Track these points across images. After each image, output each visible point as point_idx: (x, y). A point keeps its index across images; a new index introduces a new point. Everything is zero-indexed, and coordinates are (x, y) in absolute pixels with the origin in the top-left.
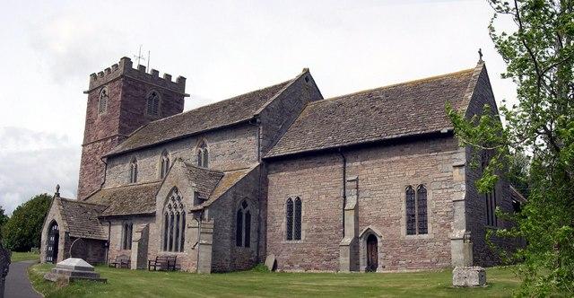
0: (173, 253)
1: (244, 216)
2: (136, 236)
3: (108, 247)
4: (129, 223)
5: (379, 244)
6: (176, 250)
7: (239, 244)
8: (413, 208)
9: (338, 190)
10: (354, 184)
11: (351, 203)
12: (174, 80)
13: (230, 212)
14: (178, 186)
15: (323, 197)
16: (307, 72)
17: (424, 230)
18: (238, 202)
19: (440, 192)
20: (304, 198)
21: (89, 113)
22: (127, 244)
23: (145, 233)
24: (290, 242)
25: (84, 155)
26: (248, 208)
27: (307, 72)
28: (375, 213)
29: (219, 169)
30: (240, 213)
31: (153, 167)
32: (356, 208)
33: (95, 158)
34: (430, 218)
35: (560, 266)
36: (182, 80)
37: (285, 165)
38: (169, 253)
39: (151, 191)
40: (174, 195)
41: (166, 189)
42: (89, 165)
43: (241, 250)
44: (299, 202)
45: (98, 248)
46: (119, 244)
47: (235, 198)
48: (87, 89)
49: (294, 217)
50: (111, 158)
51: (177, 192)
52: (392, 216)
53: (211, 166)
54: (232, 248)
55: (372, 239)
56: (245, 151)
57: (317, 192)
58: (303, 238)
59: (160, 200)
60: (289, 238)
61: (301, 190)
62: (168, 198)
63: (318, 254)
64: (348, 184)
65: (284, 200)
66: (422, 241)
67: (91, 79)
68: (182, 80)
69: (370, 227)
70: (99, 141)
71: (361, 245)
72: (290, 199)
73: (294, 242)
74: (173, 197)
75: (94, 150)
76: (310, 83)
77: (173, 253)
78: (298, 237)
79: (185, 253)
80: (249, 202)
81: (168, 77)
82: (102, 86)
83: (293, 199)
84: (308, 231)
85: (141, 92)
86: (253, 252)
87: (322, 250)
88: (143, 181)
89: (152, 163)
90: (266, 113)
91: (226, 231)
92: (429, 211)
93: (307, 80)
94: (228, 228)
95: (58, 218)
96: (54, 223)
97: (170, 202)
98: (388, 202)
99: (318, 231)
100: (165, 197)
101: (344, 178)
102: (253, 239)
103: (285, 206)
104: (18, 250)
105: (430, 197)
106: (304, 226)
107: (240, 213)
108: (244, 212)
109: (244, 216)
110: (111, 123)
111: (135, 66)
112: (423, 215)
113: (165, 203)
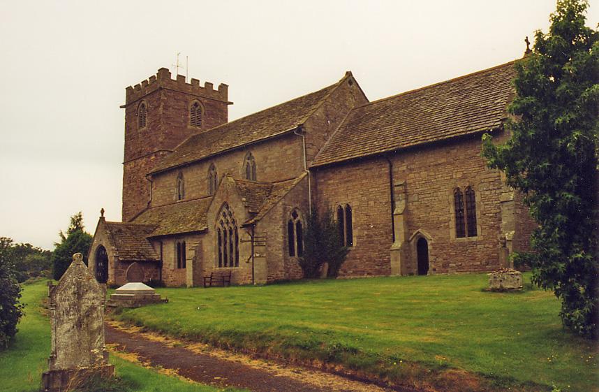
1: (295, 227)
2: (190, 254)
4: (181, 241)
5: (430, 247)
6: (225, 266)
7: (292, 254)
9: (386, 195)
10: (401, 188)
12: (216, 88)
13: (281, 223)
15: (372, 203)
16: (349, 74)
17: (473, 232)
19: (487, 193)
20: (354, 204)
23: (199, 251)
26: (299, 218)
27: (349, 74)
30: (291, 224)
32: (407, 212)
34: (479, 221)
36: (224, 87)
44: (348, 208)
46: (173, 264)
50: (157, 175)
52: (440, 219)
55: (422, 243)
58: (354, 244)
62: (219, 214)
63: (370, 259)
64: (396, 189)
66: (471, 243)
68: (224, 87)
73: (465, 239)
80: (299, 213)
81: (209, 85)
82: (141, 99)
83: (343, 206)
84: (359, 237)
85: (183, 103)
87: (374, 255)
92: (478, 213)
94: (280, 239)
97: (222, 218)
100: (216, 212)
101: (391, 182)
105: (477, 199)
106: (355, 233)
107: (291, 224)
108: (295, 222)
109: (295, 227)
111: (174, 77)
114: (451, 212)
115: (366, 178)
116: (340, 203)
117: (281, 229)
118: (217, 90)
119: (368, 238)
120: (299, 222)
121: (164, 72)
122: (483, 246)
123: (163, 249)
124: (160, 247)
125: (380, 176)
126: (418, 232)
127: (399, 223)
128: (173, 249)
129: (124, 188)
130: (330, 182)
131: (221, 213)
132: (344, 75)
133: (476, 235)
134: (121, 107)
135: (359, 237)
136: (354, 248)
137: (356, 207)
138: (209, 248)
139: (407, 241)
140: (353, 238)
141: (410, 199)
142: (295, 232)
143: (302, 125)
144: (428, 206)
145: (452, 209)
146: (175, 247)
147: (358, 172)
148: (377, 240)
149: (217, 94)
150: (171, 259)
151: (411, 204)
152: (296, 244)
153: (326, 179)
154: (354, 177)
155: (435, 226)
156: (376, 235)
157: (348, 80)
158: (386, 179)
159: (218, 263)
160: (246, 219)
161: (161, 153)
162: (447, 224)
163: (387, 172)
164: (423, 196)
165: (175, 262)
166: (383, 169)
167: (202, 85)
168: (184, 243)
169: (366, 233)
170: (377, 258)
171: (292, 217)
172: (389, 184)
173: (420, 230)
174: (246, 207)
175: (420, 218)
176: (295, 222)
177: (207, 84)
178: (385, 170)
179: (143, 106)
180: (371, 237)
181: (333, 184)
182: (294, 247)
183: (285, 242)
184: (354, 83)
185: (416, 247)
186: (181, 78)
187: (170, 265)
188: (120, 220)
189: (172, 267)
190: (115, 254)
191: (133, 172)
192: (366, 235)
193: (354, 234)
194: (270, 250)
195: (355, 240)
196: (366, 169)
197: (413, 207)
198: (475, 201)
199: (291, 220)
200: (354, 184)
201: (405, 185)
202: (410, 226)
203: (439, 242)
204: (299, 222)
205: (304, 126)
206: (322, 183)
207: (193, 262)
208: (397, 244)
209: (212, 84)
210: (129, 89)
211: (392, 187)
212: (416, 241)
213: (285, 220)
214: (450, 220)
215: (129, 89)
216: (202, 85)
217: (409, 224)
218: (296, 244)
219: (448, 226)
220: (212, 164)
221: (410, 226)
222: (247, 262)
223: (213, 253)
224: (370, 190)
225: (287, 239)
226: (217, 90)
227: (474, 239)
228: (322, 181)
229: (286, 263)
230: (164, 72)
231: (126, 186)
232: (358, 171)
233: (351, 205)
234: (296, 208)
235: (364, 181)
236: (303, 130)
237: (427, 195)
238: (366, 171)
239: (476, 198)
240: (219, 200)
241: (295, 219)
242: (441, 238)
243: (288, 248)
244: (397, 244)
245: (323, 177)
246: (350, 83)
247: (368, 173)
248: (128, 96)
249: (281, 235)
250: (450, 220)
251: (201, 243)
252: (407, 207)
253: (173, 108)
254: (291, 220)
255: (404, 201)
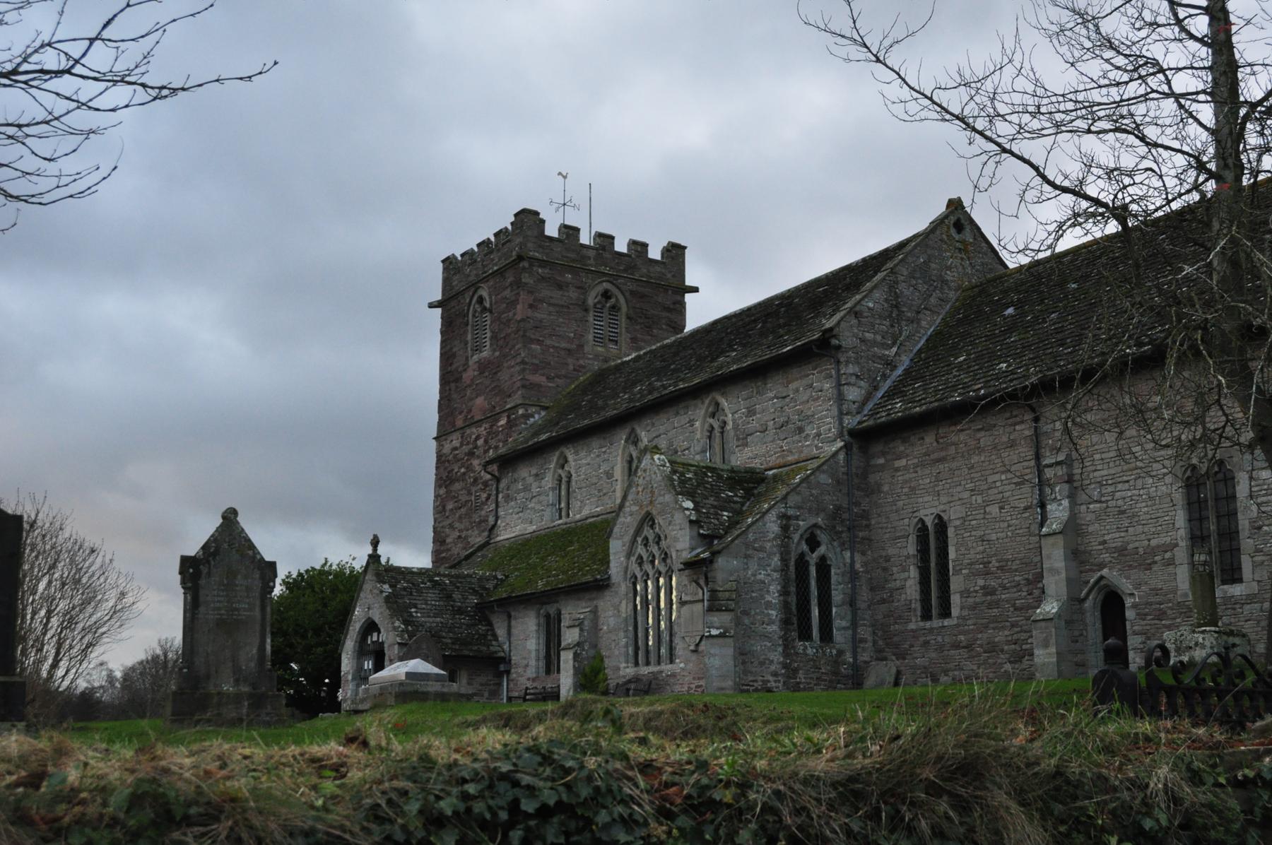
0: (653, 669)
1: (813, 571)
2: (570, 636)
3: (508, 672)
4: (552, 610)
5: (1130, 614)
6: (648, 663)
7: (805, 635)
8: (1202, 519)
9: (1026, 489)
10: (1060, 471)
11: (1058, 512)
12: (655, 253)
13: (776, 561)
14: (654, 512)
15: (994, 510)
16: (955, 205)
18: (796, 537)
20: (954, 515)
21: (447, 358)
22: (551, 664)
23: (592, 629)
24: (928, 624)
25: (441, 460)
26: (822, 550)
27: (955, 205)
28: (1114, 538)
29: (756, 464)
30: (802, 563)
31: (609, 475)
32: (1073, 528)
33: (470, 468)
34: (1247, 543)
35: (985, 652)
36: (675, 252)
37: (904, 441)
38: (645, 670)
39: (598, 531)
40: (647, 532)
41: (627, 521)
42: (457, 486)
43: (807, 649)
44: (941, 526)
45: (482, 679)
46: (533, 663)
47: (785, 528)
48: (437, 296)
49: (933, 565)
50: (509, 462)
51: (652, 527)
52: (1154, 543)
53: (741, 458)
54: (787, 646)
55: (1112, 604)
56: (809, 419)
57: (979, 499)
58: (955, 612)
59: (617, 547)
60: (926, 616)
61: (944, 499)
62: (634, 541)
63: (992, 648)
64: (1049, 473)
65: (907, 525)
67: (445, 269)
68: (675, 252)
69: (1105, 572)
70: (478, 423)
71: (1089, 619)
72: (922, 521)
73: (936, 623)
74: (646, 539)
75: (466, 449)
76: (968, 235)
77: (653, 669)
78: (946, 613)
79: (679, 665)
80: (822, 537)
81: (639, 247)
82: (475, 286)
83: (929, 522)
84: (965, 593)
85: (573, 294)
86: (840, 653)
87: (1000, 637)
88: (586, 512)
89: (604, 467)
90: (854, 321)
91: (769, 605)
92: (1243, 523)
93: (959, 227)
94: (773, 596)
95: (378, 614)
96: (371, 627)
97: (640, 550)
98: (1142, 508)
99: (987, 591)
100: (627, 538)
101: (1038, 457)
102: (840, 622)
103: (912, 539)
104: (1127, 667)
106: (956, 583)
107: (802, 563)
108: (813, 558)
109: (813, 571)
110: (504, 376)
111: (552, 230)
112: (1229, 535)
113: (629, 555)
114: (1177, 526)
115: (980, 450)
116: (921, 514)
117: (776, 575)
118: (658, 257)
119: (985, 594)
120: (823, 559)
121: (528, 220)
122: (1257, 606)
123: (514, 631)
124: (506, 624)
125: (1012, 445)
126: (1102, 578)
127: (1055, 558)
128: (534, 628)
129: (437, 496)
130: (898, 464)
131: (639, 540)
132: (944, 209)
133: (1240, 580)
134: (431, 306)
135: (965, 593)
136: (955, 622)
137: (958, 523)
138: (612, 621)
139: (1074, 601)
140: (952, 597)
141: (1082, 497)
142: (813, 583)
143: (831, 329)
144: (1123, 512)
145: (1181, 518)
146: (539, 625)
147: (962, 437)
148: (1007, 601)
149: (658, 269)
150: (530, 652)
151: (1083, 508)
152: (815, 612)
153: (889, 457)
154: (952, 450)
155: (1145, 560)
156: (1005, 588)
157: (953, 219)
158: (1026, 451)
159: (632, 659)
160: (693, 549)
161: (521, 412)
162: (1168, 555)
163: (1027, 433)
164: (1110, 489)
165: (538, 660)
166: (1017, 427)
167: (621, 246)
168: (559, 614)
169: (981, 582)
170: (1008, 643)
171: (805, 547)
172: (1033, 463)
173: (1105, 572)
174: (691, 522)
175: (1105, 542)
176: (813, 558)
177: (633, 244)
178: (1025, 430)
179: (481, 300)
180: (992, 592)
181: (906, 468)
182: (809, 619)
183: (786, 605)
184: (968, 229)
185: (1098, 614)
186: (570, 232)
187: (527, 666)
188: (430, 565)
189: (531, 672)
190: (398, 640)
191: (456, 459)
192: (983, 588)
193: (953, 587)
194: (747, 621)
195: (955, 600)
196: (979, 430)
197: (1090, 517)
198: (1234, 497)
199: (802, 555)
200: (954, 465)
201: (1068, 462)
202: (1082, 563)
203: (1152, 600)
204: (823, 559)
205: (835, 332)
206: (882, 468)
207: (576, 656)
208: (1051, 607)
209: (612, 238)
210: (449, 262)
211: (1040, 470)
212: (1101, 597)
213: (788, 553)
214: (1176, 545)
215: (449, 262)
216: (621, 246)
217: (1077, 555)
218: (815, 612)
219: (1173, 558)
220: (633, 430)
221: (1082, 563)
222: (693, 651)
223: (622, 634)
224: (991, 479)
225: (793, 599)
226: (658, 257)
227: (946, 622)
228: (881, 461)
229: (786, 654)
230: (528, 220)
231: (442, 491)
232: (960, 436)
233: (946, 518)
234: (815, 526)
235: (975, 459)
236: (834, 342)
237: (1120, 486)
238: (979, 435)
239: (1238, 488)
240: (635, 508)
241: (813, 551)
242: (1156, 591)
243: (795, 620)
244: (1051, 607)
245: (883, 454)
246: (959, 227)
247: (985, 439)
248: (447, 282)
249: (774, 588)
250: (1176, 545)
251: (595, 612)
252: (1073, 516)
253: (550, 304)
254: (802, 555)
255: (1066, 503)
